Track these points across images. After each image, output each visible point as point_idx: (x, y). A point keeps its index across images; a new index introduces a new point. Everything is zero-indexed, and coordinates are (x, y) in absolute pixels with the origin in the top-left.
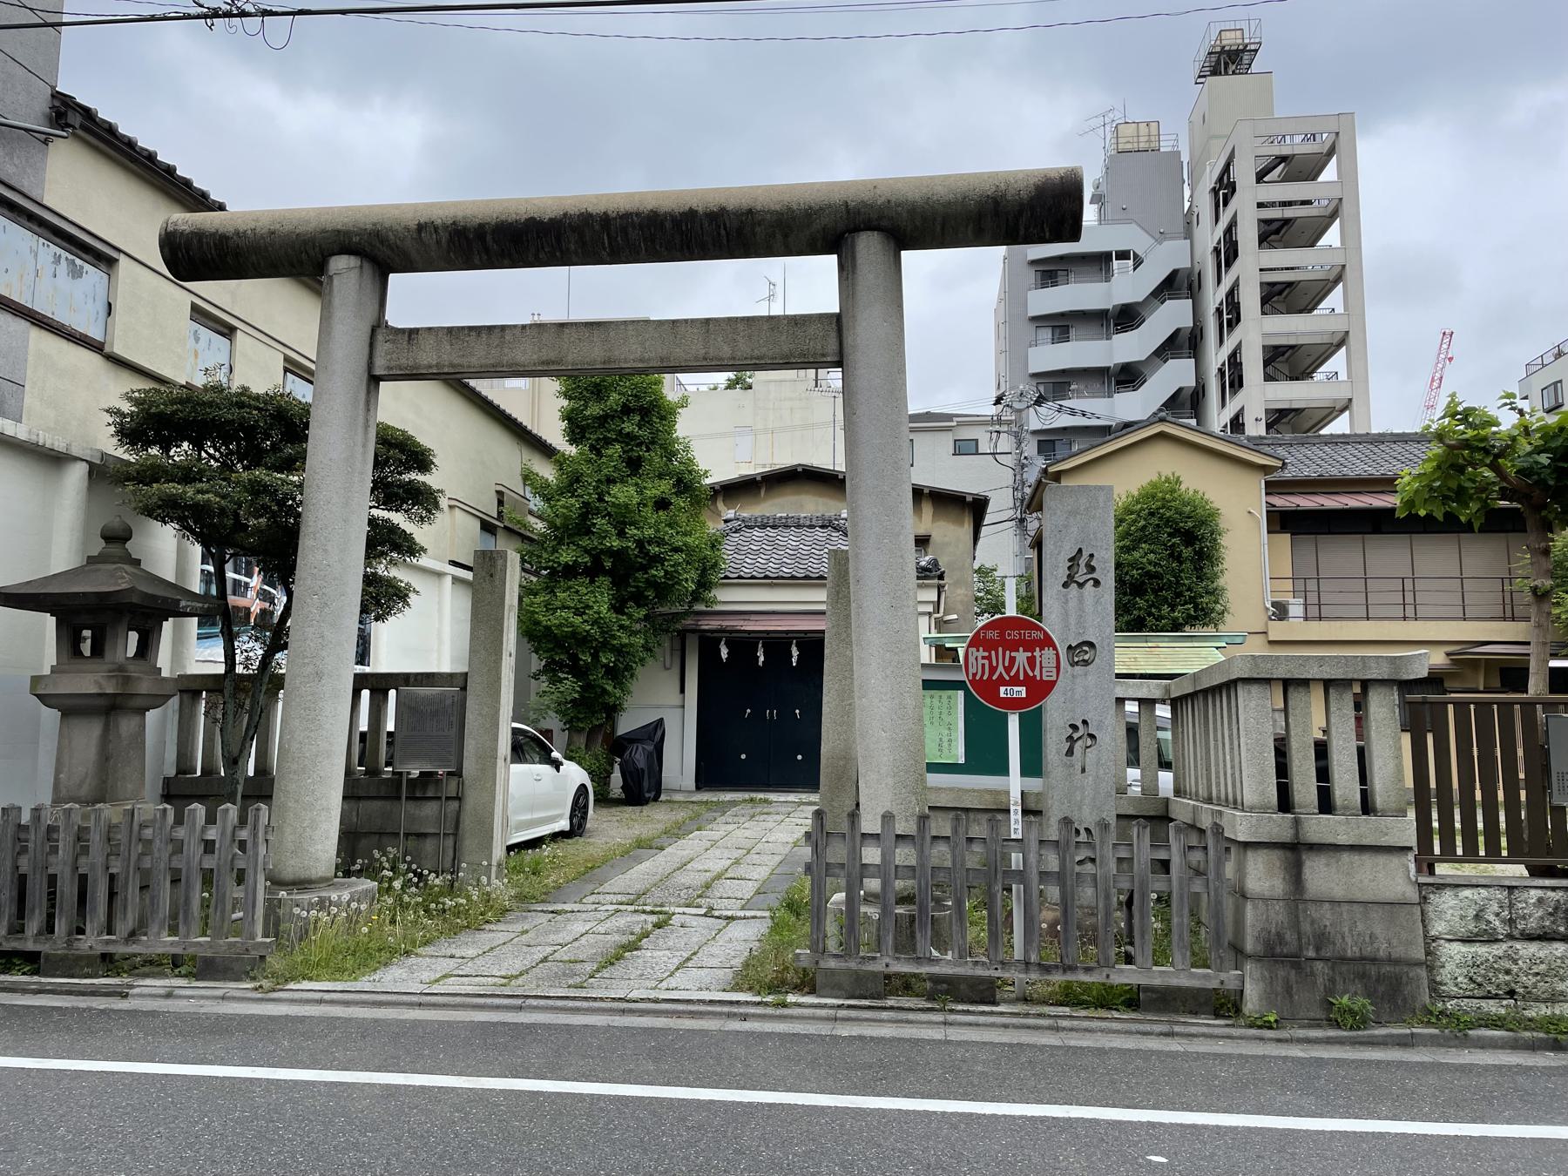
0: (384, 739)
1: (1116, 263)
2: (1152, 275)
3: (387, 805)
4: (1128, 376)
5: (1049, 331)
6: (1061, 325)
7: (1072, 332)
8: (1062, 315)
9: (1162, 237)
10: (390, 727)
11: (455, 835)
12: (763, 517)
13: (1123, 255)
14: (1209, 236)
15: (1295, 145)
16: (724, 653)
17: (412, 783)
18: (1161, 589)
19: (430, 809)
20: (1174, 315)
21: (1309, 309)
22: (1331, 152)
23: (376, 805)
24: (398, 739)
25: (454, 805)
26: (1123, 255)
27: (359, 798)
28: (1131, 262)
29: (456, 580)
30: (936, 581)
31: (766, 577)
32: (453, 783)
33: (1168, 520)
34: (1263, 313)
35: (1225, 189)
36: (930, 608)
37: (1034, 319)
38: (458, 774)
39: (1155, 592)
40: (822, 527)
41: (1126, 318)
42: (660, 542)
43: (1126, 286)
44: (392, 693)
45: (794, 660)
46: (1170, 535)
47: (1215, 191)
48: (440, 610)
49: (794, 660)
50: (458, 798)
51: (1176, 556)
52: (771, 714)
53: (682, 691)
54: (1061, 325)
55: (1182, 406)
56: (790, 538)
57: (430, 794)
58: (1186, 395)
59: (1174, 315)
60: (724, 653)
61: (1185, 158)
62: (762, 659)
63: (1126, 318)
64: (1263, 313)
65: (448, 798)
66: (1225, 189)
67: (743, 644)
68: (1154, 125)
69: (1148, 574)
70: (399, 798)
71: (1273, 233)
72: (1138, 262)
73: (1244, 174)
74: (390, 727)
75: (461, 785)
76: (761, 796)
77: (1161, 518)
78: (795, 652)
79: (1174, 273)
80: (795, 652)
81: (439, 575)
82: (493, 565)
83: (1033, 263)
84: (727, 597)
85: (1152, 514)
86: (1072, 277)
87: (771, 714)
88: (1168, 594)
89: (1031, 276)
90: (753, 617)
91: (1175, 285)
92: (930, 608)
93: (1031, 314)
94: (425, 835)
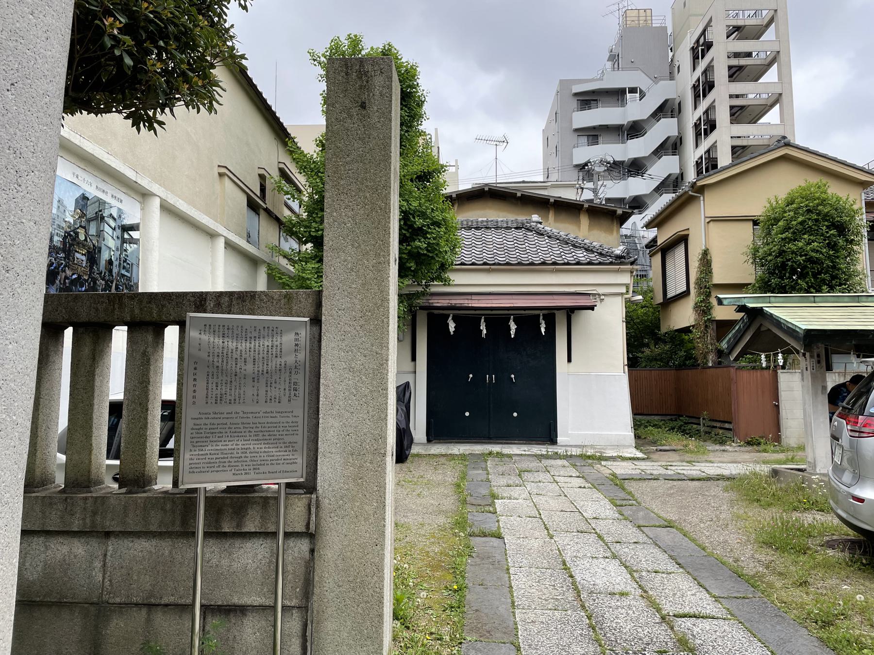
0: (156, 414)
1: (628, 95)
2: (652, 103)
3: (165, 547)
4: (636, 167)
5: (586, 138)
6: (593, 134)
7: (600, 139)
8: (594, 128)
9: (656, 80)
10: (169, 392)
11: (305, 608)
12: (467, 221)
13: (633, 90)
14: (688, 77)
15: (745, 19)
16: (452, 326)
17: (215, 503)
18: (820, 273)
19: (251, 556)
20: (665, 128)
21: (754, 120)
22: (771, 21)
23: (142, 547)
24: (188, 417)
25: (303, 546)
26: (633, 90)
27: (108, 534)
28: (638, 95)
29: (229, 245)
30: (629, 267)
31: (485, 264)
32: (299, 504)
33: (826, 215)
34: (731, 123)
35: (702, 48)
36: (624, 290)
37: (576, 130)
38: (308, 486)
39: (815, 276)
40: (516, 228)
41: (635, 130)
42: (423, 215)
43: (635, 110)
44: (172, 333)
45: (513, 332)
46: (828, 227)
47: (693, 49)
48: (213, 272)
49: (513, 332)
50: (310, 535)
51: (833, 246)
52: (491, 378)
53: (414, 359)
54: (593, 134)
55: (669, 186)
56: (491, 236)
57: (250, 526)
58: (673, 178)
59: (665, 128)
60: (452, 326)
61: (669, 31)
62: (485, 332)
63: (635, 130)
64: (731, 123)
65: (287, 535)
66: (702, 48)
67: (468, 319)
68: (648, 12)
69: (811, 260)
70: (193, 534)
71: (735, 73)
72: (642, 95)
73: (717, 35)
74: (169, 392)
75: (313, 508)
76: (496, 448)
77: (818, 214)
78: (513, 327)
79: (666, 101)
80: (513, 327)
81: (212, 235)
82: (366, 87)
83: (576, 94)
84: (460, 281)
85: (809, 211)
86: (600, 104)
87: (491, 378)
88: (827, 277)
89: (574, 103)
90: (474, 297)
91: (666, 109)
92: (624, 290)
93: (575, 126)
94: (241, 610)
